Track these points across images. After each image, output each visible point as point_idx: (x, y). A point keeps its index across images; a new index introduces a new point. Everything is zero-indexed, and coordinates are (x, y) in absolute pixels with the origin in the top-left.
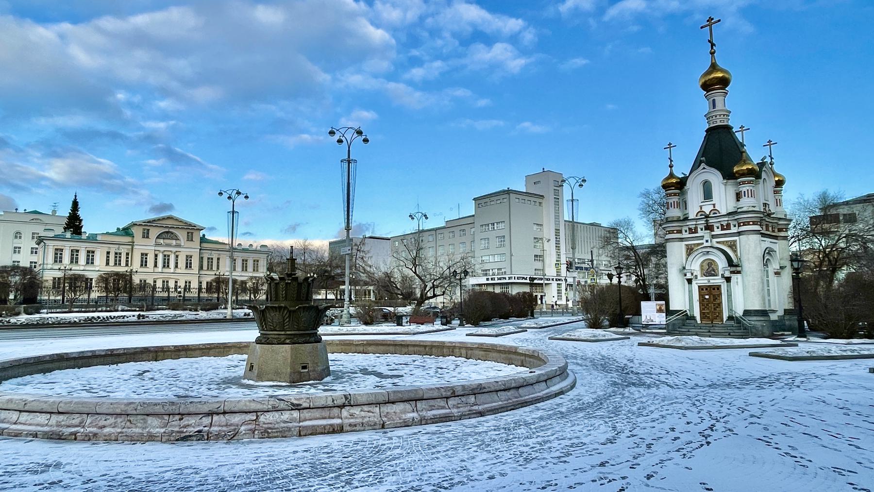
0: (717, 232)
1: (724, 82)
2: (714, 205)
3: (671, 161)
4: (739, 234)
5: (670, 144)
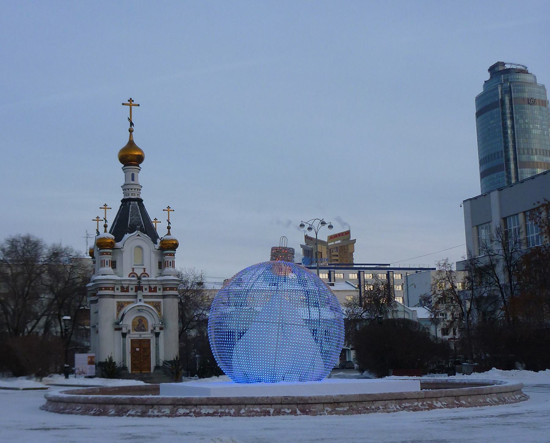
0: (146, 293)
1: (140, 159)
2: (144, 269)
3: (169, 223)
4: (164, 297)
5: (105, 205)
